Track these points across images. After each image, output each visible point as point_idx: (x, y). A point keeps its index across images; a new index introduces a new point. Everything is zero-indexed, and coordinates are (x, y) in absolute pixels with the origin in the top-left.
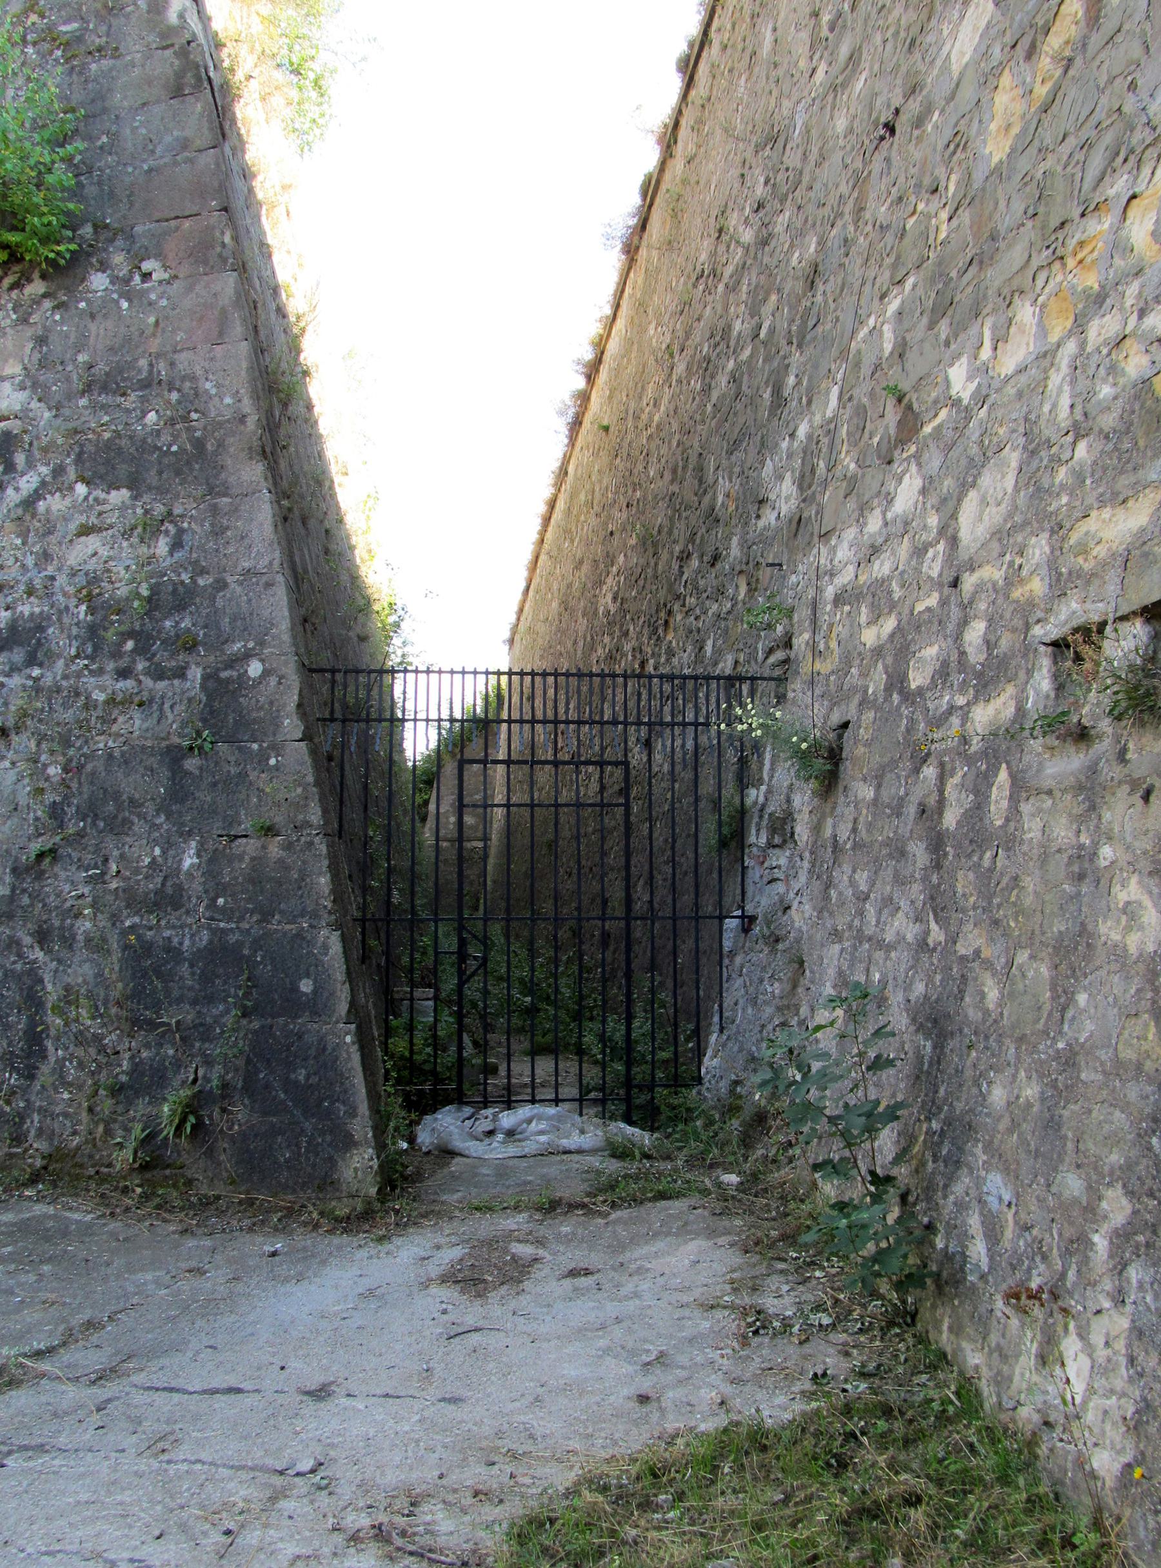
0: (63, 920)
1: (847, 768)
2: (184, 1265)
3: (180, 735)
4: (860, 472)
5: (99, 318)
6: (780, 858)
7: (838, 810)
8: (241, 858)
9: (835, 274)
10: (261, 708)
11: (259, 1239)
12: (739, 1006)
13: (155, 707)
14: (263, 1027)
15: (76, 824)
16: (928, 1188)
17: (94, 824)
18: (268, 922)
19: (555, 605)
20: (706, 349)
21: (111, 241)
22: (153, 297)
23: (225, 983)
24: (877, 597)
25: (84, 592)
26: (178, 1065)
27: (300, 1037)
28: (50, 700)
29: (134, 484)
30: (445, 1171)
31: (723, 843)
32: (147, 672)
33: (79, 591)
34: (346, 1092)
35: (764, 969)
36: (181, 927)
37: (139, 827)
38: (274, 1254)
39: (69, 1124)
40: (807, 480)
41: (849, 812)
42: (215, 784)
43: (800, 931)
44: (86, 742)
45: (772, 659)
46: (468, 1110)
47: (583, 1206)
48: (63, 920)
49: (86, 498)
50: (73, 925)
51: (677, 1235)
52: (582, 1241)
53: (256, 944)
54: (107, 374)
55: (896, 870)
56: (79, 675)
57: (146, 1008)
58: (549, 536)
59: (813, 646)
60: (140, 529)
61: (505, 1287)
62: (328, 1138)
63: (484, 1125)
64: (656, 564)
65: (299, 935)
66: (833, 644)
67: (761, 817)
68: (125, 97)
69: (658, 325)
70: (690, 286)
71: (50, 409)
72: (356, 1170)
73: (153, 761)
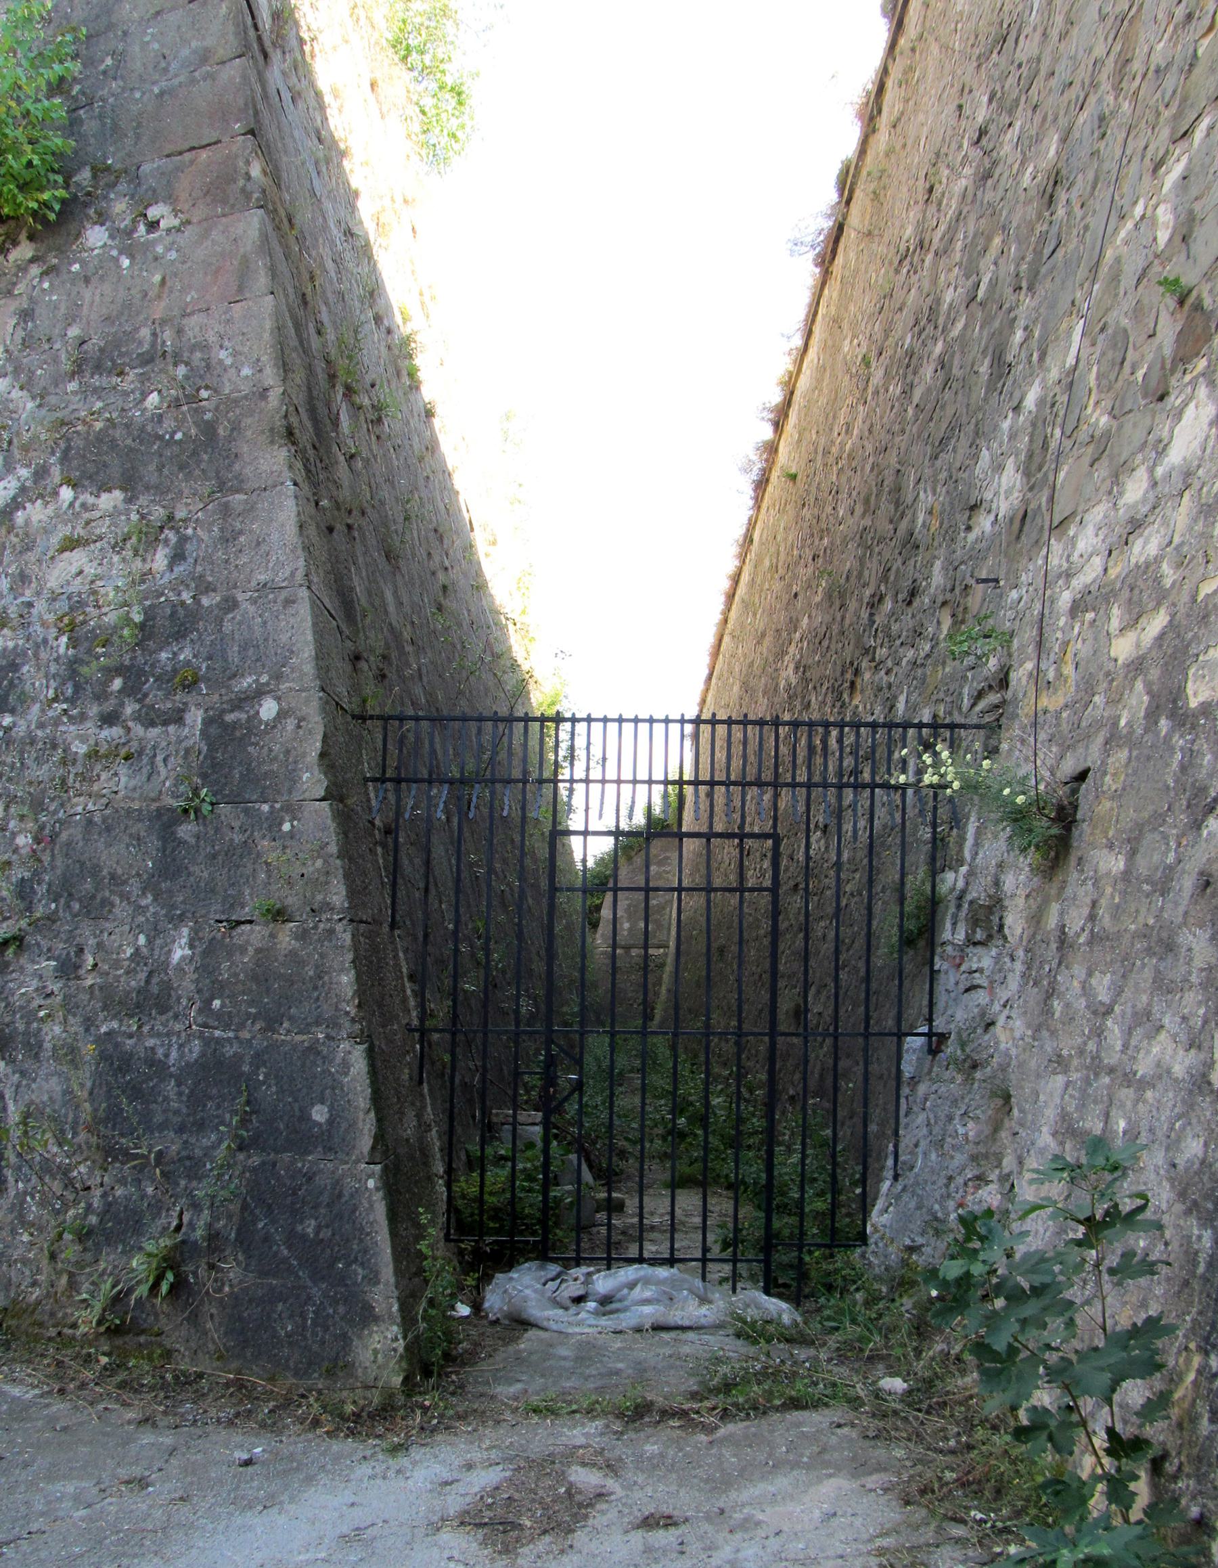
0: (28, 1024)
1: (1084, 832)
2: (123, 1473)
3: (176, 797)
4: (1115, 423)
5: (94, 280)
6: (984, 959)
7: (1069, 891)
8: (243, 950)
9: (1083, 171)
10: (275, 758)
11: (237, 1438)
12: (920, 1150)
13: (145, 760)
14: (263, 1163)
15: (47, 905)
16: (1199, 1459)
17: (68, 906)
18: (274, 1031)
19: (736, 688)
20: (908, 341)
21: (114, 185)
22: (160, 249)
23: (218, 1107)
24: (1139, 591)
25: (66, 620)
26: (157, 1208)
27: (310, 1178)
28: (22, 753)
29: (130, 484)
30: (511, 1349)
31: (907, 941)
32: (137, 717)
33: (61, 619)
34: (366, 1251)
35: (955, 1103)
36: (168, 1035)
37: (121, 910)
38: (248, 1463)
39: (27, 1273)
40: (1037, 459)
41: (1085, 894)
42: (214, 857)
43: (1007, 1054)
44: (62, 805)
45: (978, 708)
46: (554, 1269)
47: (683, 1414)
48: (28, 1024)
49: (71, 505)
50: (40, 1030)
51: (809, 1467)
52: (672, 1468)
53: (258, 1059)
54: (102, 350)
55: (1158, 971)
56: (57, 722)
57: (122, 1135)
58: (733, 615)
59: (1037, 675)
60: (134, 539)
61: (547, 1538)
62: (341, 1309)
63: (572, 1288)
64: (843, 618)
65: (313, 1049)
66: (1069, 670)
67: (959, 907)
68: (135, 8)
69: (854, 337)
70: (892, 273)
71: (33, 398)
72: (376, 1352)
73: (140, 828)
